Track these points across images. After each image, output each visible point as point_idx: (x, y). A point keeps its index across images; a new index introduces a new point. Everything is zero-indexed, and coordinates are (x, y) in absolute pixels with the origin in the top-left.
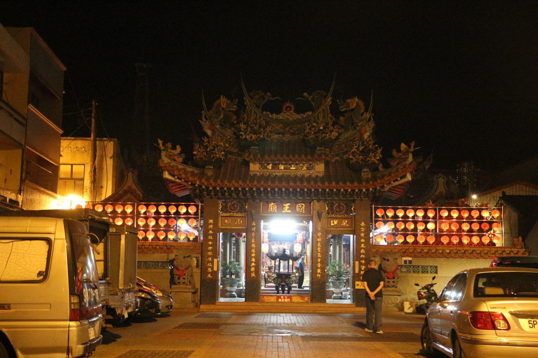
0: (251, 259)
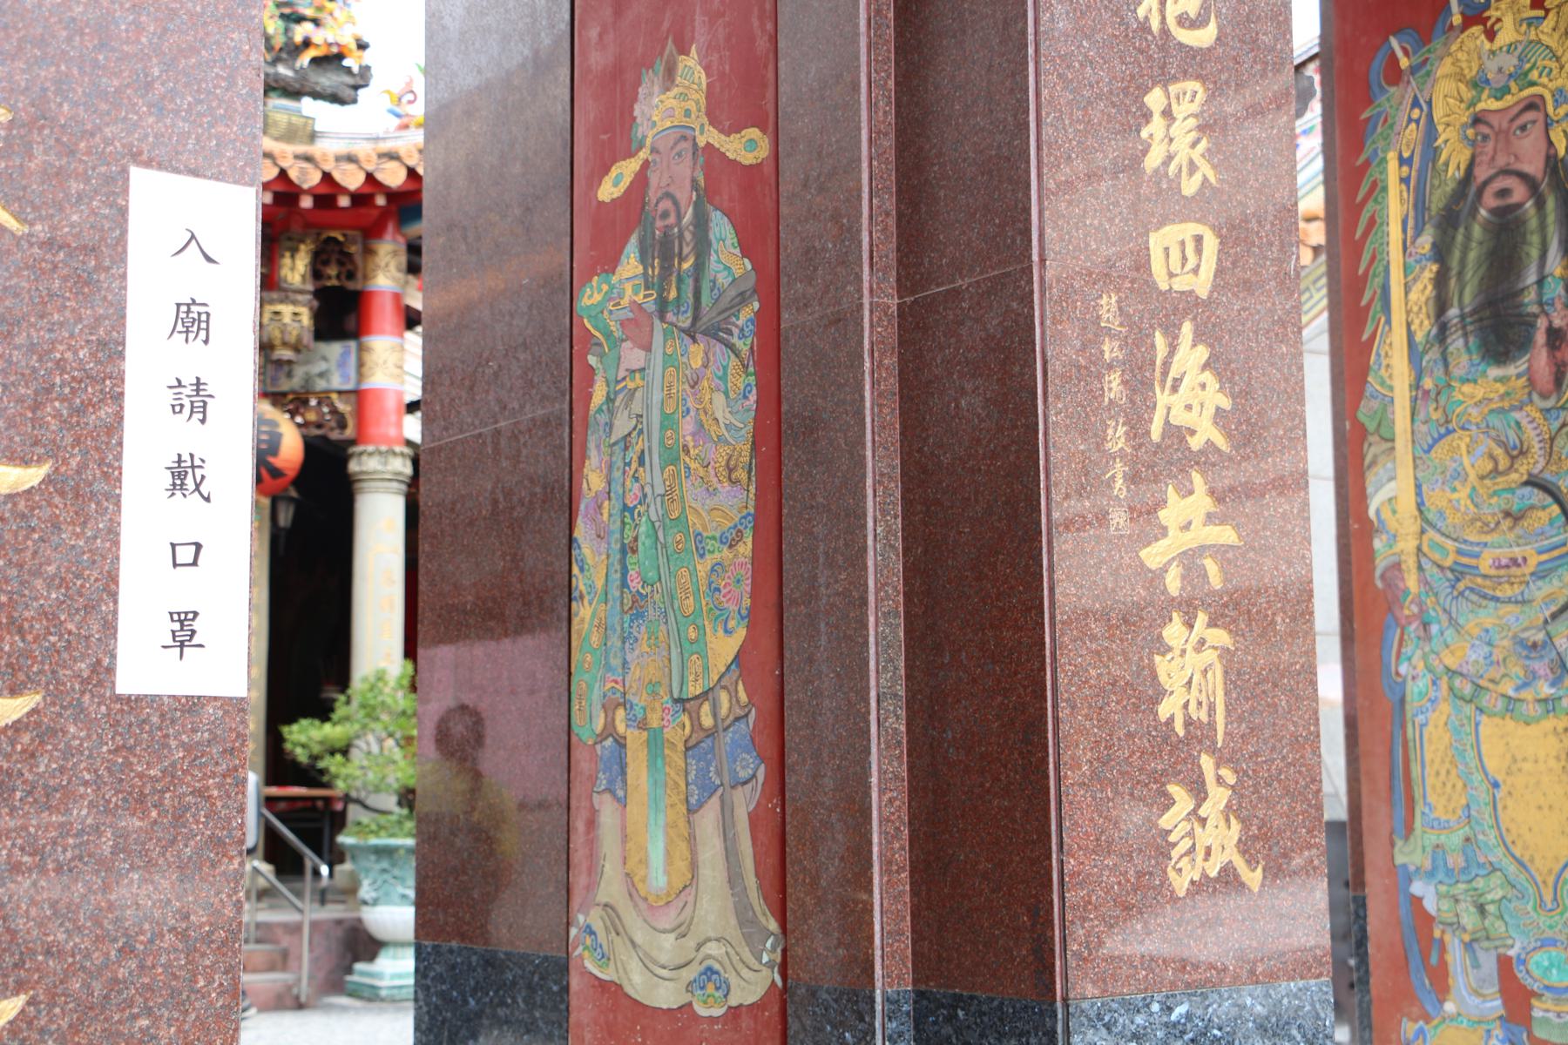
0: (1143, 377)
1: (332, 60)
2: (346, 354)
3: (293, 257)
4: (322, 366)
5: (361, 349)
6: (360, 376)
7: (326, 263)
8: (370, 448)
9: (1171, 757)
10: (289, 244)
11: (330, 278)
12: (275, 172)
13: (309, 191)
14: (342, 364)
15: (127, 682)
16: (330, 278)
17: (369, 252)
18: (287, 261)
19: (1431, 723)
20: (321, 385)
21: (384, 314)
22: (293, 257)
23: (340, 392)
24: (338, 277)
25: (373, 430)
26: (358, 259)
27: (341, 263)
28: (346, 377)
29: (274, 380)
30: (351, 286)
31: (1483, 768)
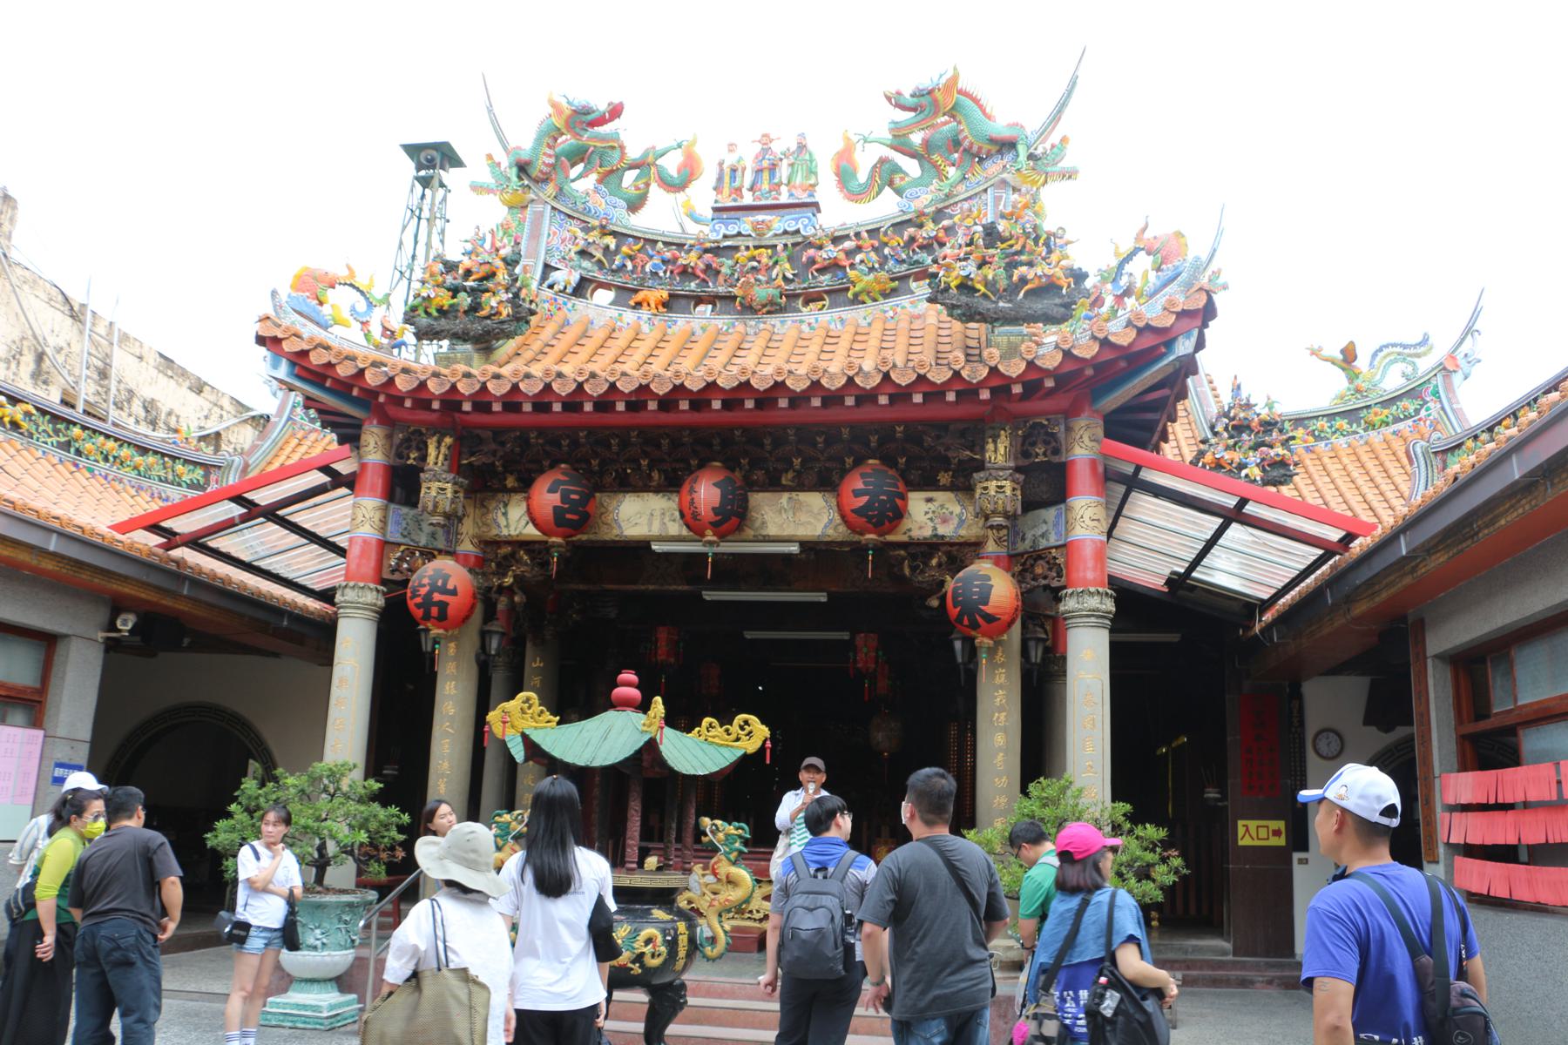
1: (1049, 288)
2: (1058, 516)
3: (995, 442)
4: (1045, 528)
5: (1069, 509)
6: (1067, 532)
7: (1034, 444)
8: (1070, 591)
9: (1005, 730)
10: (990, 432)
11: (1037, 455)
12: (1023, 366)
13: (1019, 379)
14: (1056, 525)
15: (1241, 843)
16: (1037, 455)
17: (1069, 429)
18: (990, 446)
19: (515, 179)
20: (1043, 544)
21: (1082, 477)
22: (995, 442)
23: (1057, 547)
24: (1045, 454)
25: (1074, 576)
26: (1062, 436)
27: (1046, 443)
28: (1059, 534)
29: (1014, 543)
30: (1056, 459)
31: (362, 293)
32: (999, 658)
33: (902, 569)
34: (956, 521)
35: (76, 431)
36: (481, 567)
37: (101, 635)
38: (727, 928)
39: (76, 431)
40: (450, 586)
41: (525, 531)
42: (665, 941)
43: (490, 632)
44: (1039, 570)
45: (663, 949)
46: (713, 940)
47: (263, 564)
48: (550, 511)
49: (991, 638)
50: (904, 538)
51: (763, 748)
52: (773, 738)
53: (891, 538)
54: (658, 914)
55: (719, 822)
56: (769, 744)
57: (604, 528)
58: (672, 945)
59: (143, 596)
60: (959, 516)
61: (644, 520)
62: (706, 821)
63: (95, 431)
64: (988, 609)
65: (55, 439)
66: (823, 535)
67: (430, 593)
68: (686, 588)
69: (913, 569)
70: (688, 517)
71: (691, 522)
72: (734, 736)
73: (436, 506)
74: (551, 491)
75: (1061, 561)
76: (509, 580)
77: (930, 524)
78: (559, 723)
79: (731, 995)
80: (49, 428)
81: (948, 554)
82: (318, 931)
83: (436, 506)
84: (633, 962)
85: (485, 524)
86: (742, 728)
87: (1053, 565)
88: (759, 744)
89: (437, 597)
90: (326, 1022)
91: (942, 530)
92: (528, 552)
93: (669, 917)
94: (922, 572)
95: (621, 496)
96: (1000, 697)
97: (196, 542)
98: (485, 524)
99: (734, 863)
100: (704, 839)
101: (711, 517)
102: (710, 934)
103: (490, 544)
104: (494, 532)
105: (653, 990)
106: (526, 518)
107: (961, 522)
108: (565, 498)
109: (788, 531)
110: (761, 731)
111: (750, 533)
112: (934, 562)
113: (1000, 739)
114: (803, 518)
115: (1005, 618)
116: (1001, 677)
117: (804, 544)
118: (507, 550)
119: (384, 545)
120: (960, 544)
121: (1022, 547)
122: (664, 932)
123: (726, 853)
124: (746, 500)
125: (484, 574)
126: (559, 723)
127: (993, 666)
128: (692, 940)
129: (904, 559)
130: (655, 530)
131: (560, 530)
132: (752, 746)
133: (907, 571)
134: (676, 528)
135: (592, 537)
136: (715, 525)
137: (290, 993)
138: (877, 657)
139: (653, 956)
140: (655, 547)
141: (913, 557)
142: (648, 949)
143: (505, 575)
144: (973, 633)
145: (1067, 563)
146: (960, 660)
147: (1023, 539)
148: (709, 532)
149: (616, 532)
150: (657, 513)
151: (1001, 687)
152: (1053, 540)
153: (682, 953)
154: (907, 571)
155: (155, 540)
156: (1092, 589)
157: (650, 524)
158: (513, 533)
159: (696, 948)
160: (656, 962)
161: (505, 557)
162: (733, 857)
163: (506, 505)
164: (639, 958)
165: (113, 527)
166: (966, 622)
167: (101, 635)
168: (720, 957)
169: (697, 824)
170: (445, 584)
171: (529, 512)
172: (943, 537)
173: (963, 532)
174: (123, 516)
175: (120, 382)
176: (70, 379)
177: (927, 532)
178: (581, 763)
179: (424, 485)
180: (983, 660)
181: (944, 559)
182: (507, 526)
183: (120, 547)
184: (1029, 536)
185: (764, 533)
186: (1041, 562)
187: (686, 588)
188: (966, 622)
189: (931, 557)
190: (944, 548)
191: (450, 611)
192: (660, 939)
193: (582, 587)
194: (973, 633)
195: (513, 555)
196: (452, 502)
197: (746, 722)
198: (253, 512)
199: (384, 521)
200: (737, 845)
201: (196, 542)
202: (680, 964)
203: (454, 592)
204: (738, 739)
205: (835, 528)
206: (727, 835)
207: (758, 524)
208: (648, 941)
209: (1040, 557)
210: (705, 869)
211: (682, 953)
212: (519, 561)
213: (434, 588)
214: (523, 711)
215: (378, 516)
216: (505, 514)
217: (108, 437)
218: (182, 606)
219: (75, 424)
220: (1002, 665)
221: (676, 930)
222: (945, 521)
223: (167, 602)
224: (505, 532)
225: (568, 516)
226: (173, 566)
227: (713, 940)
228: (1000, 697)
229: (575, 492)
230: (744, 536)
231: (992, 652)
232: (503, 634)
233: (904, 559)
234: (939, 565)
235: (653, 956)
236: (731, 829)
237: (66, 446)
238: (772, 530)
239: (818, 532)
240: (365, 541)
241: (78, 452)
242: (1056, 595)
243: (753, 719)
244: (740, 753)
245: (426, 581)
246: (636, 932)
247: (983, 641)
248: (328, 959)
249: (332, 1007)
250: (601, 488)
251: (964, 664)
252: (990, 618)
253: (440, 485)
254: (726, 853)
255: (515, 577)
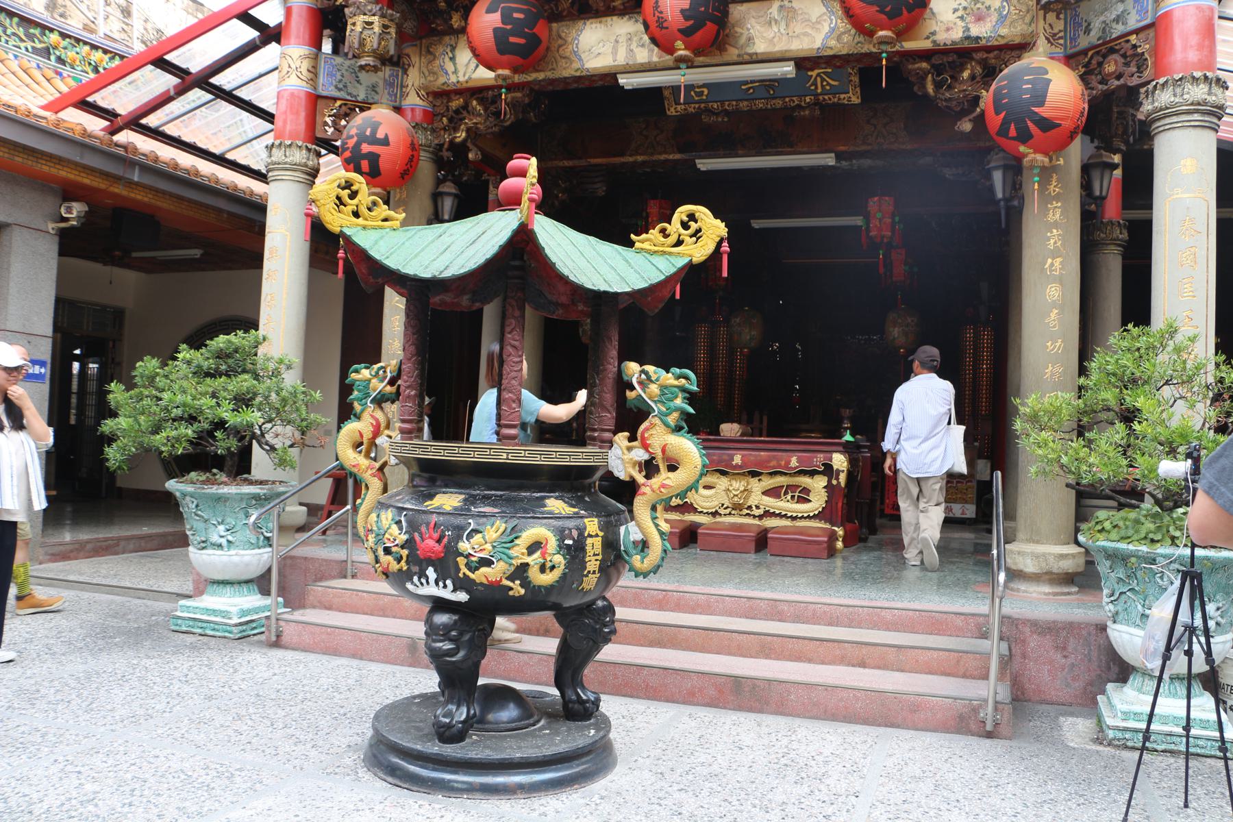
9: (1060, 280)
20: (1119, 29)
23: (1137, 32)
29: (1073, 40)
32: (1054, 188)
33: (924, 87)
34: (995, 17)
35: (54, 38)
36: (431, 122)
37: (51, 226)
38: (665, 527)
39: (54, 38)
40: (380, 135)
41: (474, 76)
42: (561, 546)
43: (441, 194)
44: (1110, 68)
45: (559, 559)
46: (644, 545)
47: (229, 156)
48: (489, 34)
49: (1046, 154)
50: (926, 45)
51: (717, 252)
52: (731, 238)
53: (909, 45)
54: (555, 505)
55: (650, 369)
56: (725, 247)
57: (563, 63)
58: (575, 552)
59: (87, 181)
60: (999, 11)
61: (608, 48)
62: (633, 367)
63: (78, 40)
64: (1044, 112)
65: (29, 45)
66: (825, 47)
67: (358, 144)
68: (678, 156)
69: (938, 85)
70: (653, 25)
71: (657, 33)
72: (673, 239)
73: (362, 43)
74: (489, 11)
75: (1144, 48)
76: (461, 135)
77: (961, 24)
78: (404, 223)
79: (706, 609)
80: (21, 32)
81: (984, 63)
82: (221, 528)
83: (362, 43)
84: (511, 578)
85: (432, 73)
86: (685, 226)
87: (1135, 58)
88: (711, 247)
89: (366, 148)
90: (235, 630)
91: (975, 31)
92: (481, 101)
93: (569, 510)
94: (950, 87)
95: (581, 23)
96: (1054, 238)
97: (135, 123)
98: (432, 73)
99: (678, 429)
100: (630, 395)
101: (684, 24)
102: (639, 537)
103: (440, 95)
104: (442, 80)
105: (563, 615)
106: (474, 62)
107: (1002, 19)
108: (506, 18)
109: (779, 47)
110: (714, 228)
111: (733, 53)
112: (966, 74)
113: (1053, 292)
114: (798, 28)
115: (1067, 124)
116: (1055, 214)
117: (804, 63)
118: (456, 103)
119: (315, 100)
120: (1000, 48)
121: (1084, 42)
122: (561, 534)
123: (662, 416)
124: (726, 13)
125: (433, 131)
126: (404, 223)
127: (1046, 199)
128: (611, 545)
129: (926, 73)
130: (621, 59)
131: (506, 58)
132: (699, 251)
133: (930, 89)
134: (645, 53)
135: (550, 75)
136: (686, 33)
137: (204, 597)
138: (893, 224)
139: (543, 569)
140: (624, 81)
141: (938, 69)
142: (534, 559)
143: (456, 129)
144: (1022, 149)
145: (1156, 51)
146: (1000, 195)
147: (1088, 31)
148: (679, 44)
149: (576, 65)
150: (622, 39)
151: (1056, 225)
152: (1133, 22)
153: (592, 564)
154: (930, 89)
155: (96, 125)
156: (1198, 74)
157: (615, 52)
158: (461, 79)
159: (619, 557)
160: (548, 579)
161: (457, 112)
162: (672, 419)
163: (453, 49)
164: (521, 571)
165: (44, 108)
166: (1013, 132)
167: (51, 226)
168: (656, 569)
169: (620, 372)
170: (374, 132)
171: (476, 55)
172: (978, 38)
173: (1004, 31)
174: (51, 95)
175: (146, 21)
176: (90, 15)
177: (957, 34)
178: (426, 274)
179: (350, 21)
180: (1033, 185)
181: (978, 70)
182: (455, 72)
183: (43, 123)
184: (1096, 25)
185: (750, 50)
186: (1115, 56)
187: (678, 156)
188: (1013, 132)
189: (962, 68)
190: (978, 56)
191: (383, 164)
192: (552, 543)
193: (566, 163)
194: (1022, 149)
195: (466, 107)
196: (381, 38)
197: (692, 217)
198: (188, 81)
199: (314, 71)
200: (679, 402)
201: (135, 123)
202: (590, 582)
203: (385, 142)
204: (679, 243)
205: (839, 38)
206: (663, 388)
207: (743, 40)
208: (534, 547)
209: (1112, 51)
210: (632, 438)
211: (592, 564)
212: (473, 113)
213: (362, 139)
214: (340, 201)
215: (305, 65)
216: (452, 59)
217: (94, 47)
218: (139, 196)
219: (52, 30)
220: (1057, 197)
221: (581, 531)
222: (979, 19)
223: (118, 189)
224: (453, 79)
225: (512, 39)
226: (121, 152)
227: (644, 545)
228: (1054, 238)
229: (518, 10)
230: (726, 58)
231: (1046, 173)
232: (456, 196)
233: (926, 73)
234: (973, 77)
235: (543, 569)
236: (668, 378)
237: (46, 52)
238: (760, 47)
239: (818, 44)
240: (292, 95)
241: (60, 60)
242: (1132, 96)
243: (702, 212)
244: (681, 262)
245: (354, 131)
246: (512, 535)
247: (1033, 157)
248: (236, 559)
249: (244, 613)
250: (556, 17)
251: (1006, 200)
252: (1046, 125)
253: (367, 18)
254: (662, 416)
255: (468, 130)
